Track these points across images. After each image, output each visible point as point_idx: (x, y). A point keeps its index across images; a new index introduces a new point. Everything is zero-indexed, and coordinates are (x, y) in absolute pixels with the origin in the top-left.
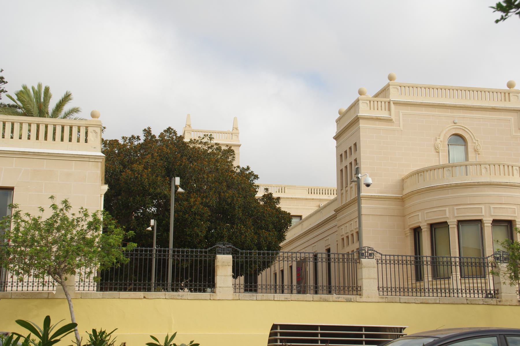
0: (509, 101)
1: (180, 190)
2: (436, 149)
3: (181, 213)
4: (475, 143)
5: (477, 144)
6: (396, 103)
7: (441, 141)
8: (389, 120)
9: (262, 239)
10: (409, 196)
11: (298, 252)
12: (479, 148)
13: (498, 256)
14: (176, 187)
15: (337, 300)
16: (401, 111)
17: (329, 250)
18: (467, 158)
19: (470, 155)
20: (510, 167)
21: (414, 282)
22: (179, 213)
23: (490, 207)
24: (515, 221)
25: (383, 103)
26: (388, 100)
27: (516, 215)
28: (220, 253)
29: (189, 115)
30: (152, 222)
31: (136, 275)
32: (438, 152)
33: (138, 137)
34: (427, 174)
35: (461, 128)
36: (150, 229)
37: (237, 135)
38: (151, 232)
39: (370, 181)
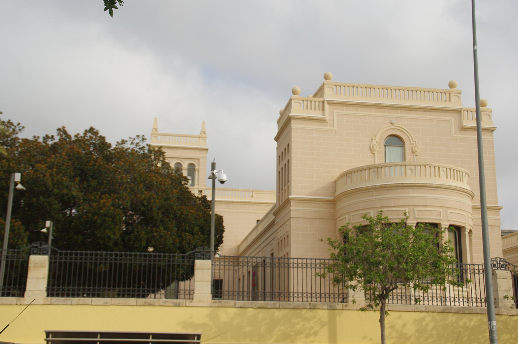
0: (450, 101)
1: (20, 186)
2: (371, 150)
3: (90, 215)
4: (413, 144)
5: (414, 145)
6: (330, 103)
7: (377, 142)
8: (322, 121)
9: (184, 243)
10: (339, 198)
11: (254, 257)
12: (416, 149)
13: (495, 263)
14: (16, 184)
15: (164, 304)
16: (335, 111)
17: (272, 255)
18: (404, 159)
19: (407, 156)
20: (437, 169)
21: (332, 286)
22: (115, 216)
23: (414, 210)
24: (440, 224)
25: (317, 103)
26: (322, 99)
27: (442, 218)
28: (199, 258)
29: (156, 119)
30: (48, 223)
31: (144, 281)
32: (374, 153)
33: (53, 136)
34: (354, 176)
35: (399, 128)
36: (44, 230)
37: (204, 138)
38: (46, 235)
39: (224, 177)
